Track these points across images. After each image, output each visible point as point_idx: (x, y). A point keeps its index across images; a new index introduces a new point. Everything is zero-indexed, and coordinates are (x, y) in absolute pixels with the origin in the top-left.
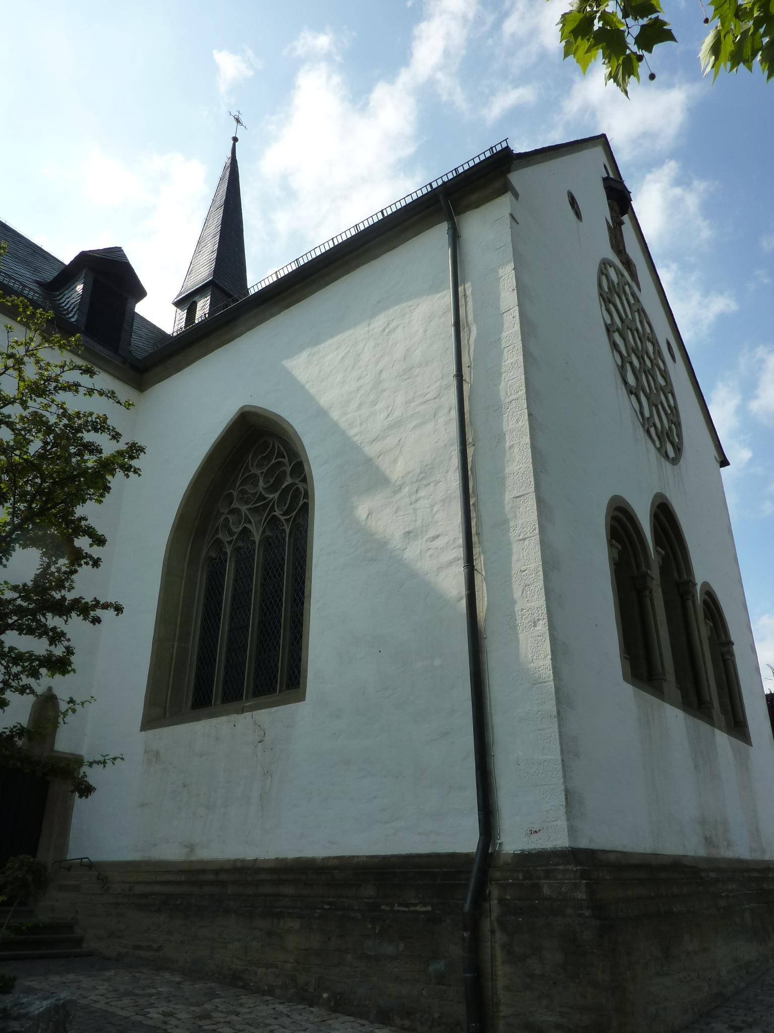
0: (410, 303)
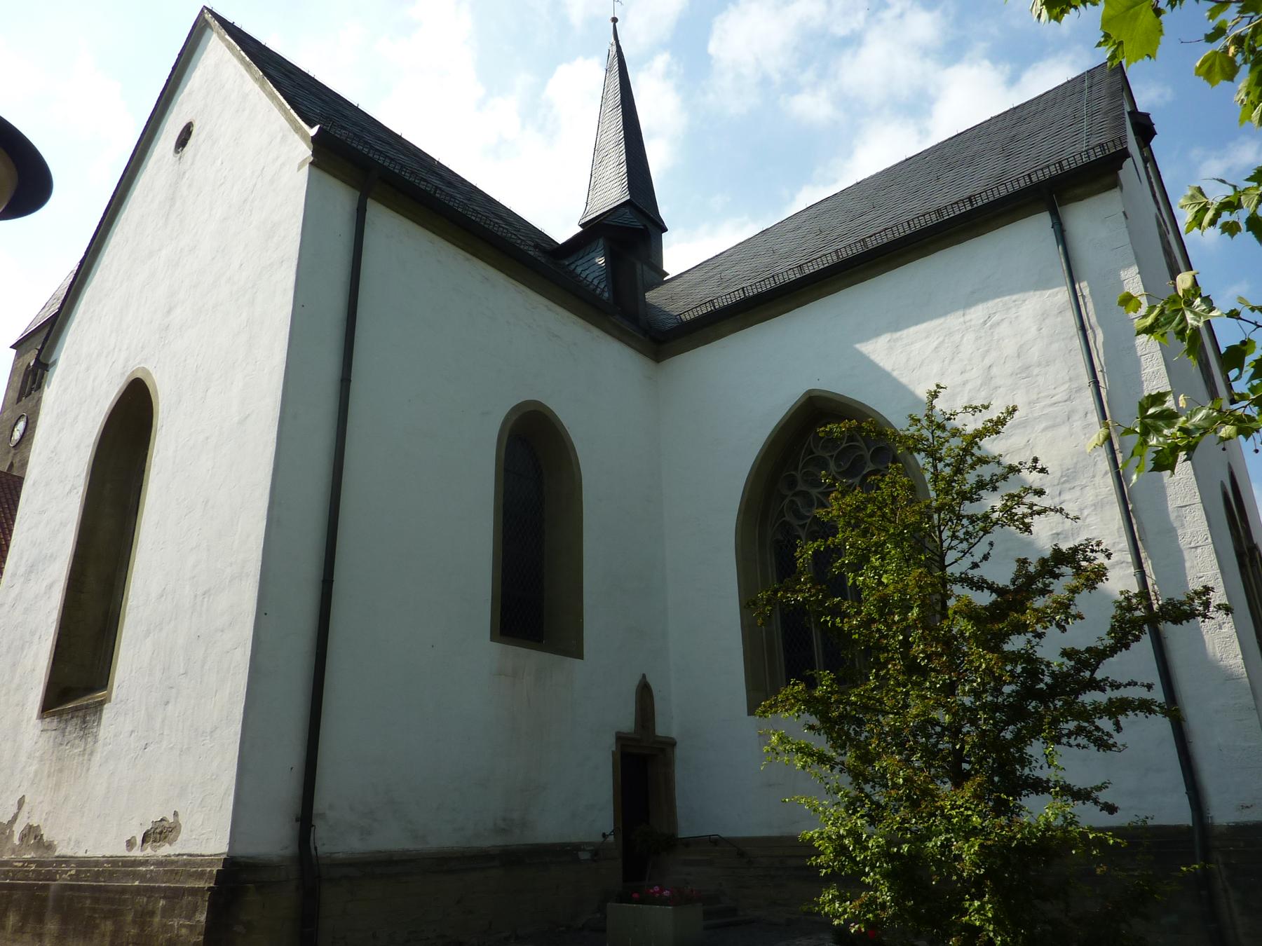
0: (1014, 297)
